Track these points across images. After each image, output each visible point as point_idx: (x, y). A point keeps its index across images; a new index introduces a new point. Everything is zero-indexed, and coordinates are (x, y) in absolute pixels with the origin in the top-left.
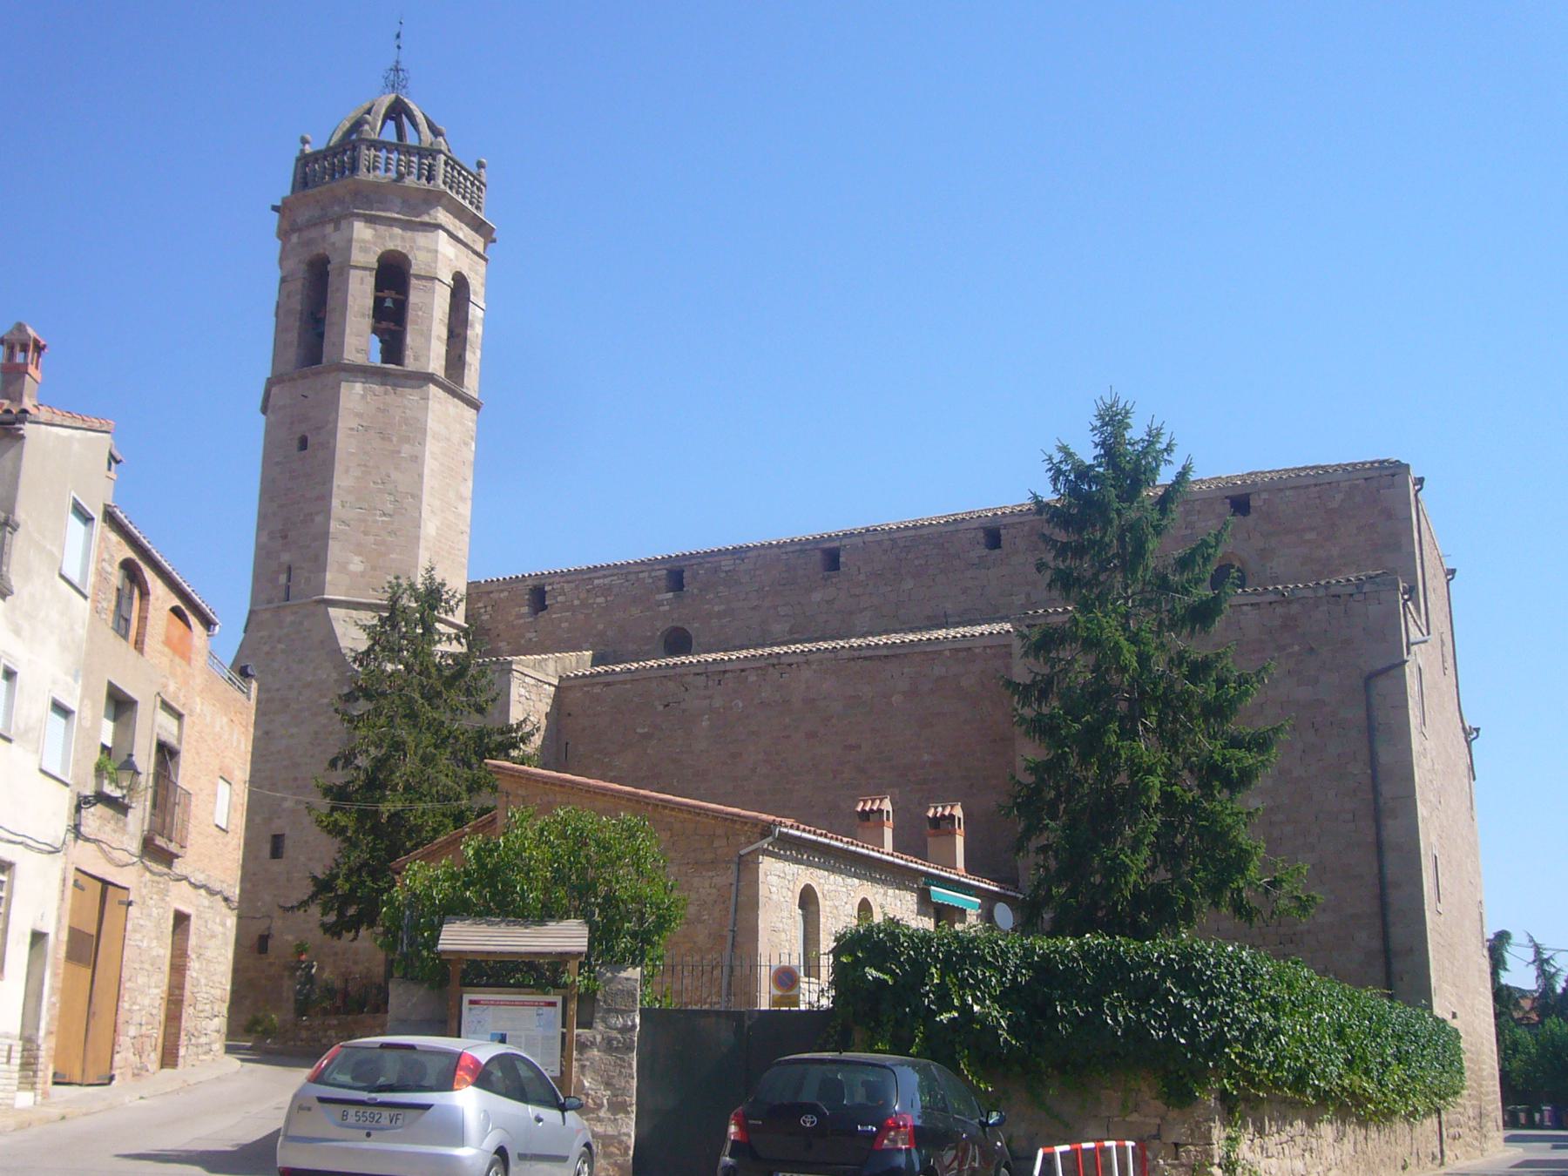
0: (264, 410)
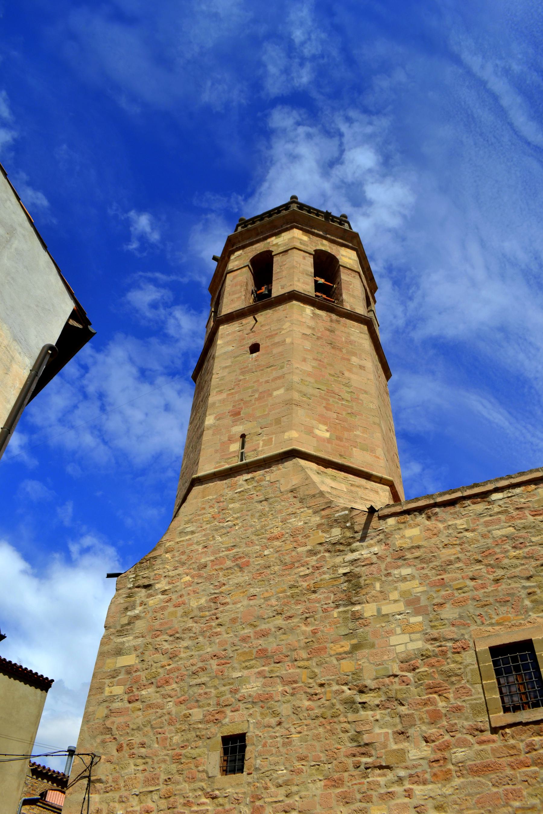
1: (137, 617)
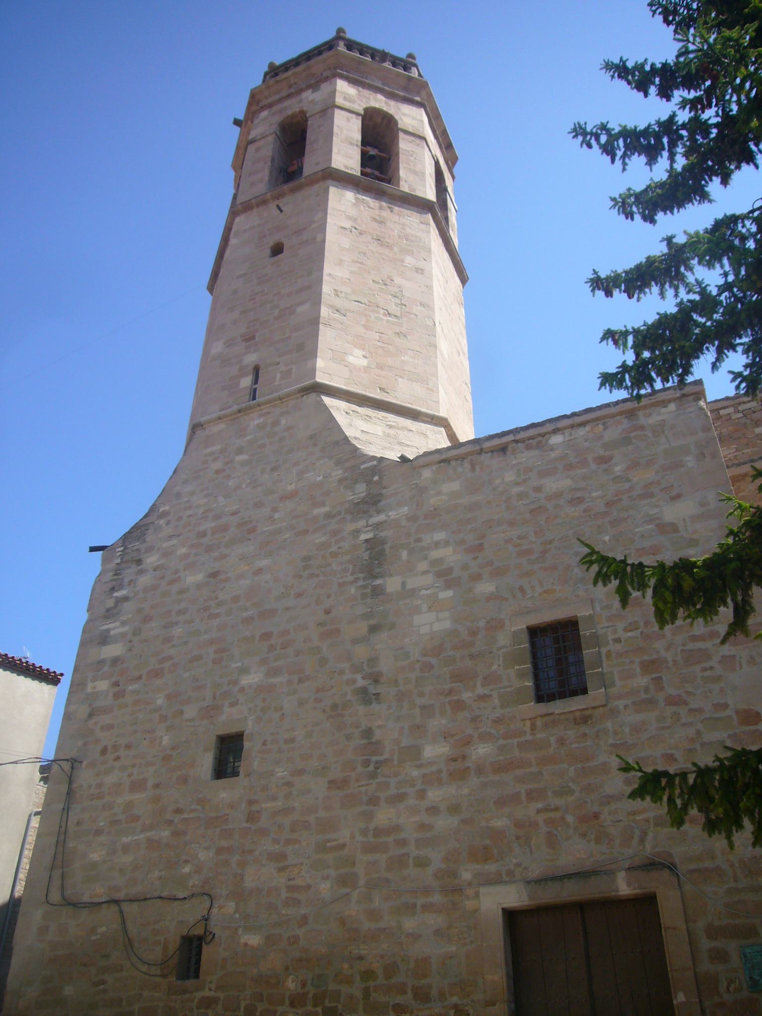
0: (211, 288)
1: (126, 599)
